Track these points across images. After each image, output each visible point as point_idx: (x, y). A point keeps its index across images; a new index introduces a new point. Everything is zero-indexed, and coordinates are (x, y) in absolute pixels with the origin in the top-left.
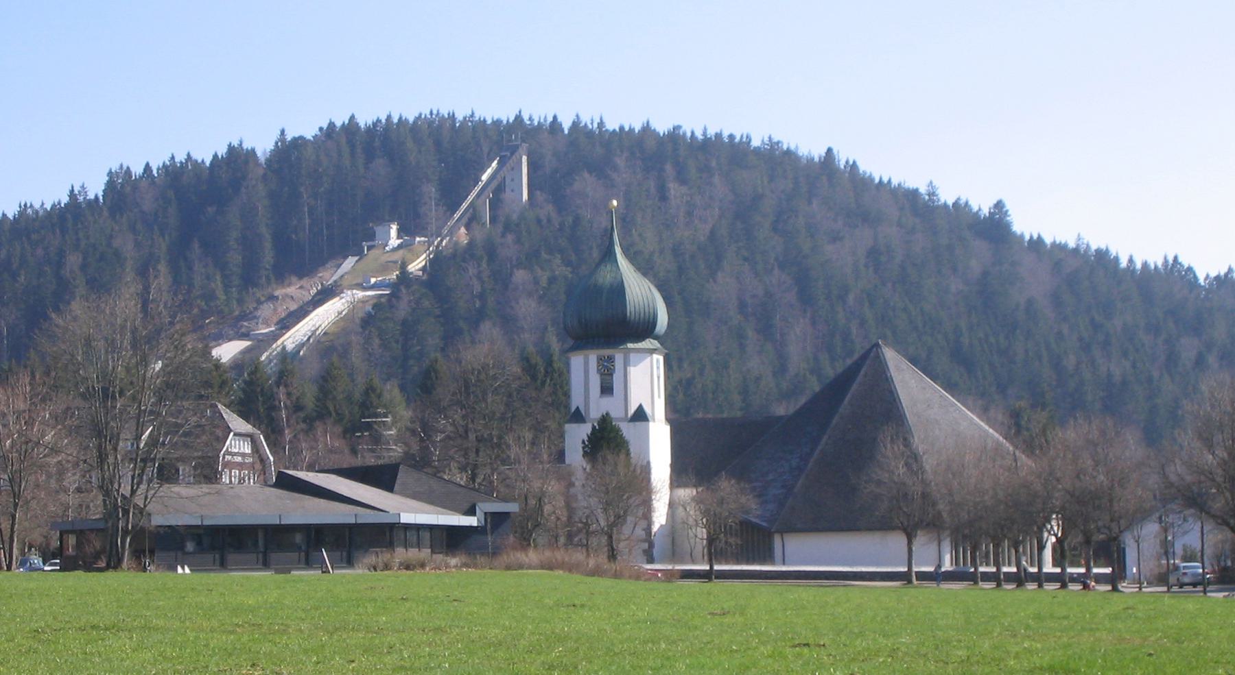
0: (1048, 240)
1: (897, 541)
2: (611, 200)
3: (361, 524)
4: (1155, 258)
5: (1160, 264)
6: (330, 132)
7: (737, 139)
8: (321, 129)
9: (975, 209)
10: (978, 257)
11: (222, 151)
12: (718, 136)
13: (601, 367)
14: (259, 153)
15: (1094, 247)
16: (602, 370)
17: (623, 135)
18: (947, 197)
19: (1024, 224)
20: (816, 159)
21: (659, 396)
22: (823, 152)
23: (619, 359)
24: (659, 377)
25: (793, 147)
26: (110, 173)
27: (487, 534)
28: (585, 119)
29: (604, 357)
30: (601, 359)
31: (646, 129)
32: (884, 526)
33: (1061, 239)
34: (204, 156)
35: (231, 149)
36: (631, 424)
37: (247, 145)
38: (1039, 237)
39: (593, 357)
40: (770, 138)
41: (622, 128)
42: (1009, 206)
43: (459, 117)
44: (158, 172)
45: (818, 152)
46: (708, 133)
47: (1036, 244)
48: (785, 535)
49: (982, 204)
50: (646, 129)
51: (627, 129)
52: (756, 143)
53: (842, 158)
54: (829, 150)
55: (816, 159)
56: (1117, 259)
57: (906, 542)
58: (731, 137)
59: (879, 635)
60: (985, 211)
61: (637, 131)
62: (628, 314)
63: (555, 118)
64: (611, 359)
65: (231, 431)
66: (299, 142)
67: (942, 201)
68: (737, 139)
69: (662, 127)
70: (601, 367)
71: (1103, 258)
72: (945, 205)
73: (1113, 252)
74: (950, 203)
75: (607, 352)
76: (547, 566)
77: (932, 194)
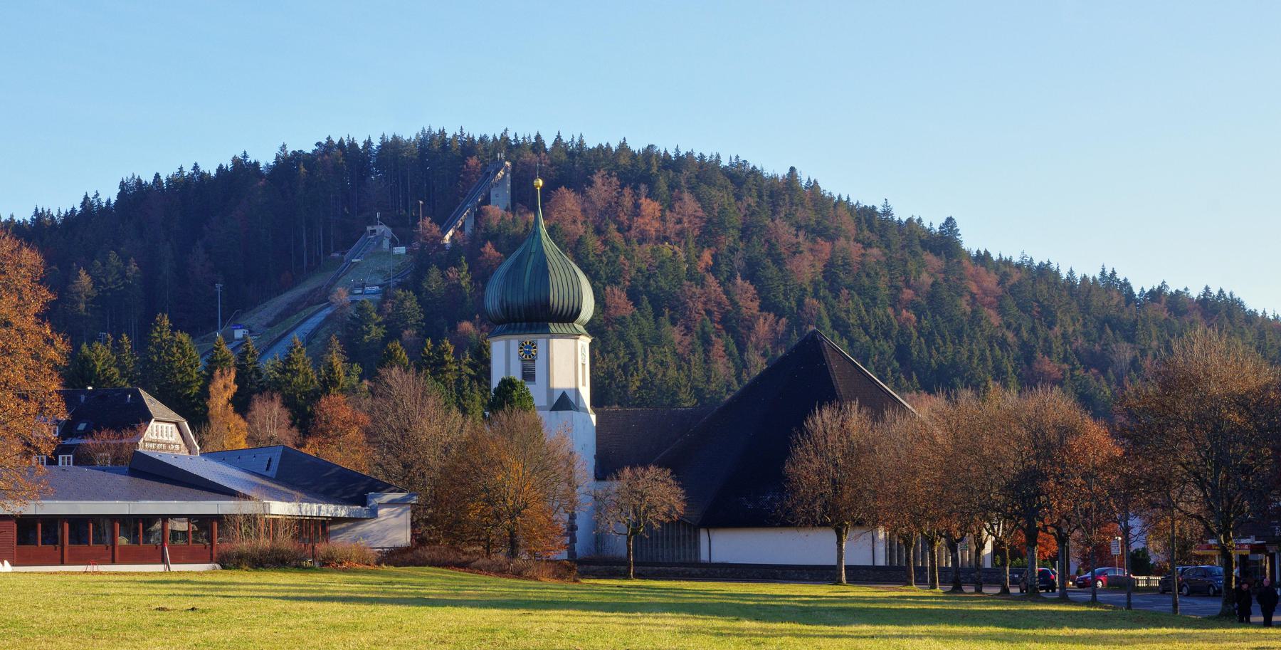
0: (995, 257)
2: (534, 178)
3: (40, 515)
4: (1093, 273)
5: (1098, 277)
6: (327, 148)
8: (318, 144)
9: (927, 226)
10: (928, 270)
11: (228, 163)
12: (690, 154)
13: (522, 353)
14: (262, 165)
17: (602, 151)
18: (901, 213)
19: (971, 242)
20: (780, 177)
21: (584, 385)
22: (787, 171)
23: (541, 342)
24: (583, 365)
26: (123, 184)
28: (566, 139)
31: (623, 146)
32: (812, 522)
33: (1006, 256)
34: (210, 168)
35: (236, 161)
36: (553, 412)
37: (252, 159)
39: (515, 342)
42: (960, 225)
43: (449, 135)
44: (167, 185)
45: (782, 172)
47: (983, 259)
48: (711, 532)
49: (933, 221)
50: (623, 146)
53: (804, 177)
54: (792, 169)
55: (780, 177)
58: (702, 156)
59: (1253, 452)
61: (614, 149)
64: (533, 345)
65: (152, 418)
66: (298, 156)
67: (896, 219)
69: (637, 146)
70: (522, 353)
71: (1044, 273)
74: (904, 219)
75: (528, 338)
77: (887, 212)
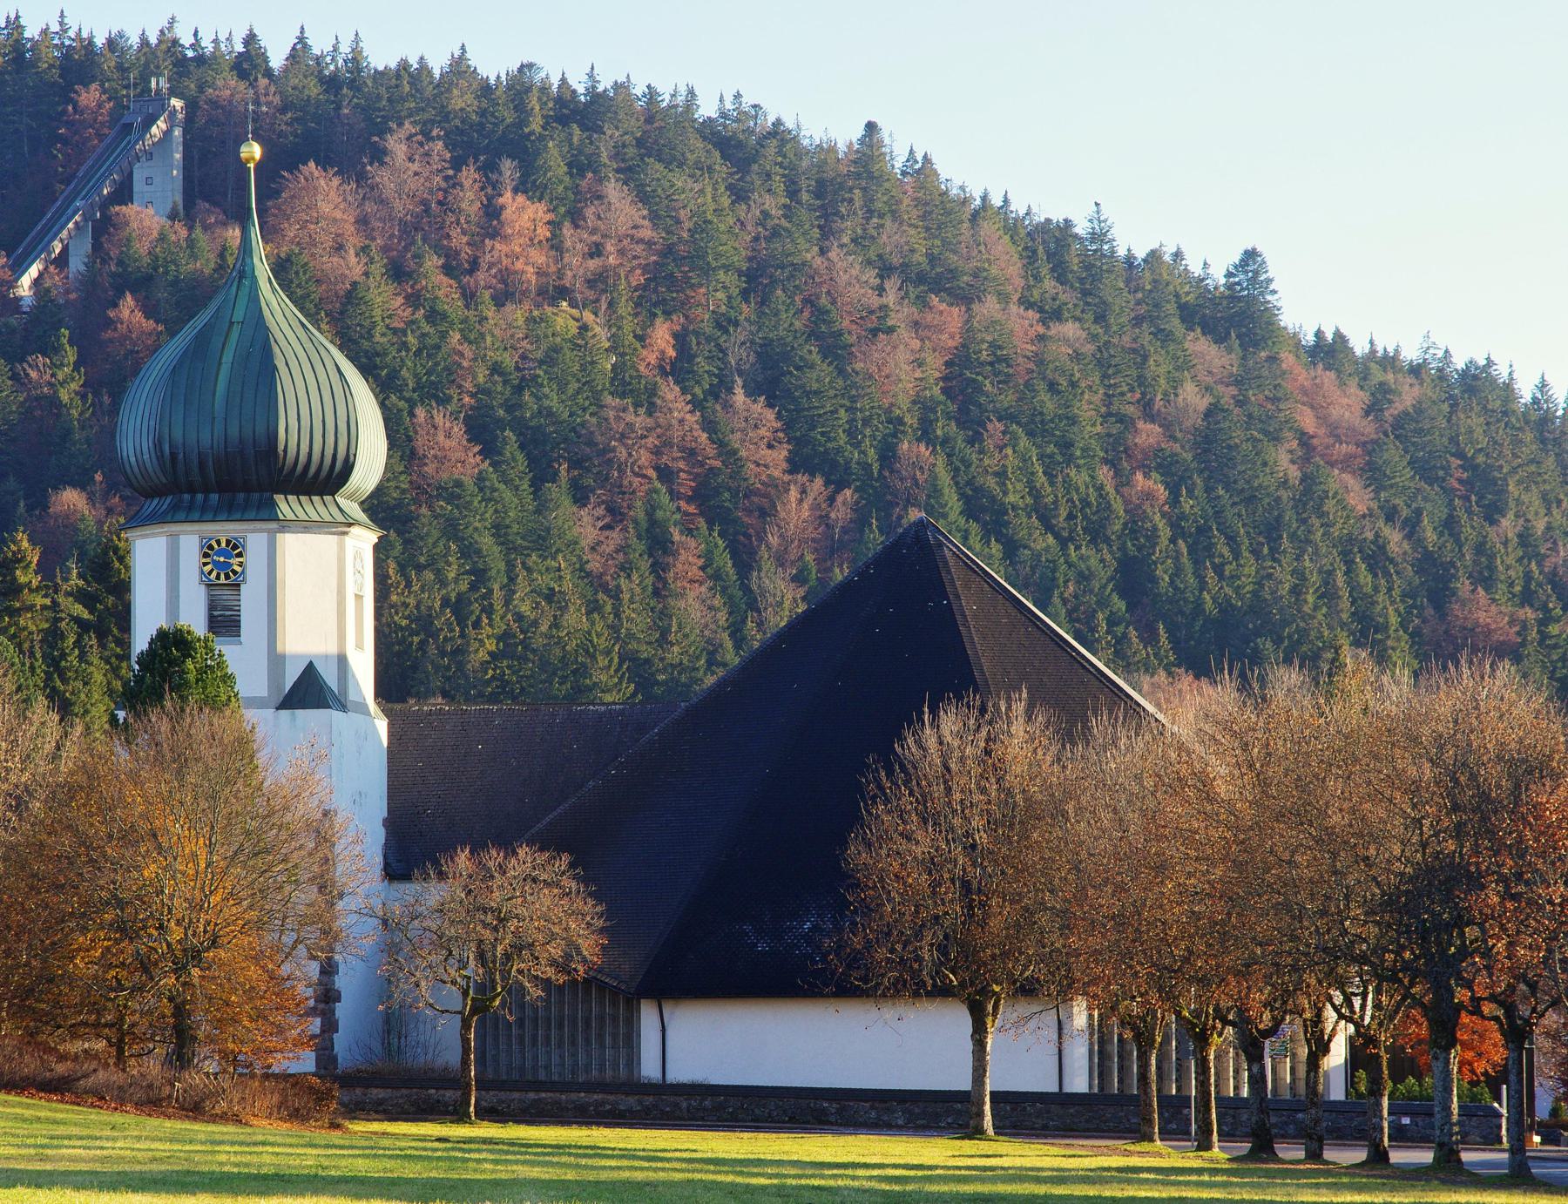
1: (954, 1020)
7: (665, 101)
15: (1459, 363)
16: (214, 574)
17: (408, 77)
24: (359, 597)
25: (790, 124)
27: (992, 1093)
29: (218, 542)
30: (211, 547)
31: (459, 67)
33: (1385, 344)
36: (285, 713)
38: (1339, 336)
39: (190, 540)
40: (738, 96)
41: (404, 65)
45: (846, 135)
46: (1012, 208)
50: (459, 67)
51: (1329, 336)
52: (707, 109)
53: (898, 148)
55: (842, 147)
56: (1508, 387)
57: (970, 1030)
58: (652, 93)
60: (1218, 276)
62: (281, 447)
63: (250, 39)
64: (235, 547)
67: (1121, 252)
68: (665, 101)
69: (493, 65)
70: (208, 568)
72: (1129, 260)
73: (1501, 372)
74: (1140, 254)
75: (224, 530)
76: (140, 1095)
77: (1098, 236)
